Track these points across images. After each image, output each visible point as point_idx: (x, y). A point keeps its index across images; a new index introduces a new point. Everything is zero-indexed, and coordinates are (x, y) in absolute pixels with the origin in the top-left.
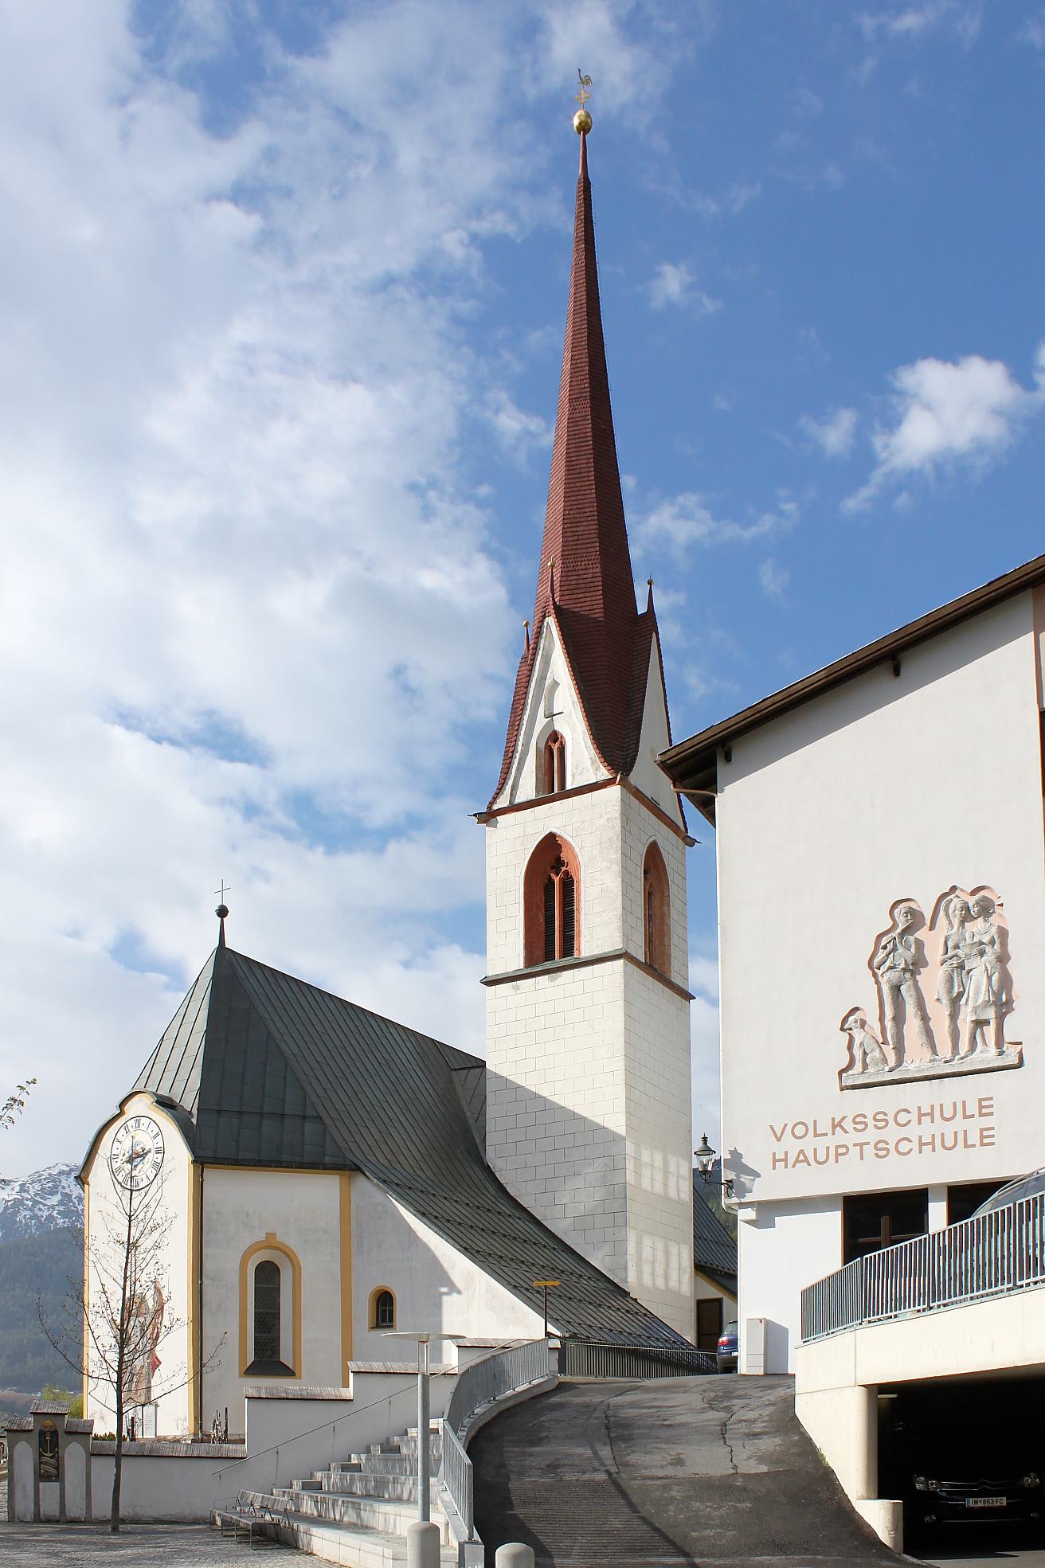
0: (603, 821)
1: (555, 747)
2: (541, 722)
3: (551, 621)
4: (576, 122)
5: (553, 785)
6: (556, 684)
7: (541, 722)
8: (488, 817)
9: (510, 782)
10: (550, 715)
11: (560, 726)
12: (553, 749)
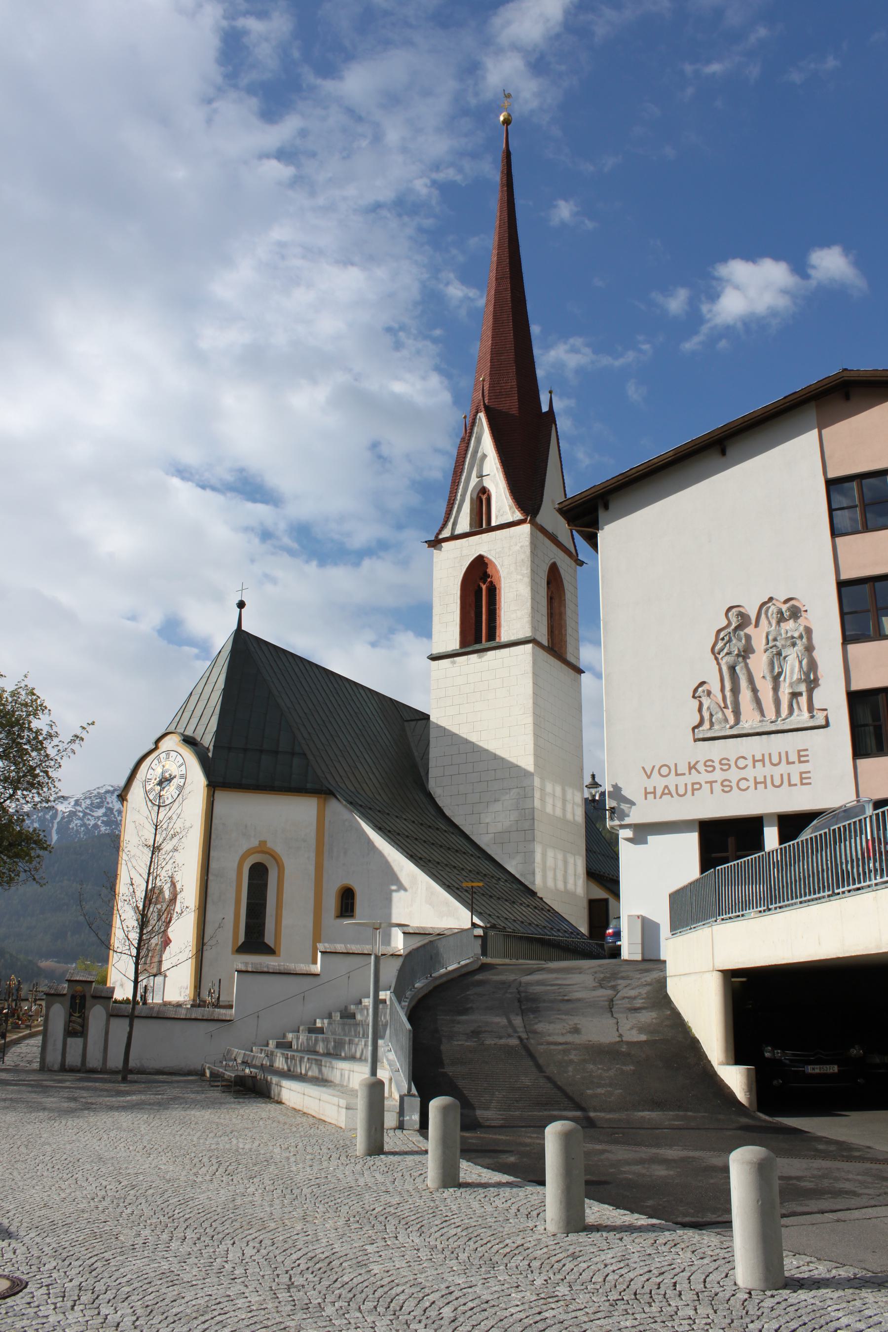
0: (518, 548)
1: (484, 497)
2: (474, 481)
3: (482, 416)
4: (502, 118)
5: (482, 523)
6: (484, 456)
7: (474, 481)
8: (436, 543)
9: (452, 520)
10: (481, 476)
11: (488, 483)
12: (482, 499)
